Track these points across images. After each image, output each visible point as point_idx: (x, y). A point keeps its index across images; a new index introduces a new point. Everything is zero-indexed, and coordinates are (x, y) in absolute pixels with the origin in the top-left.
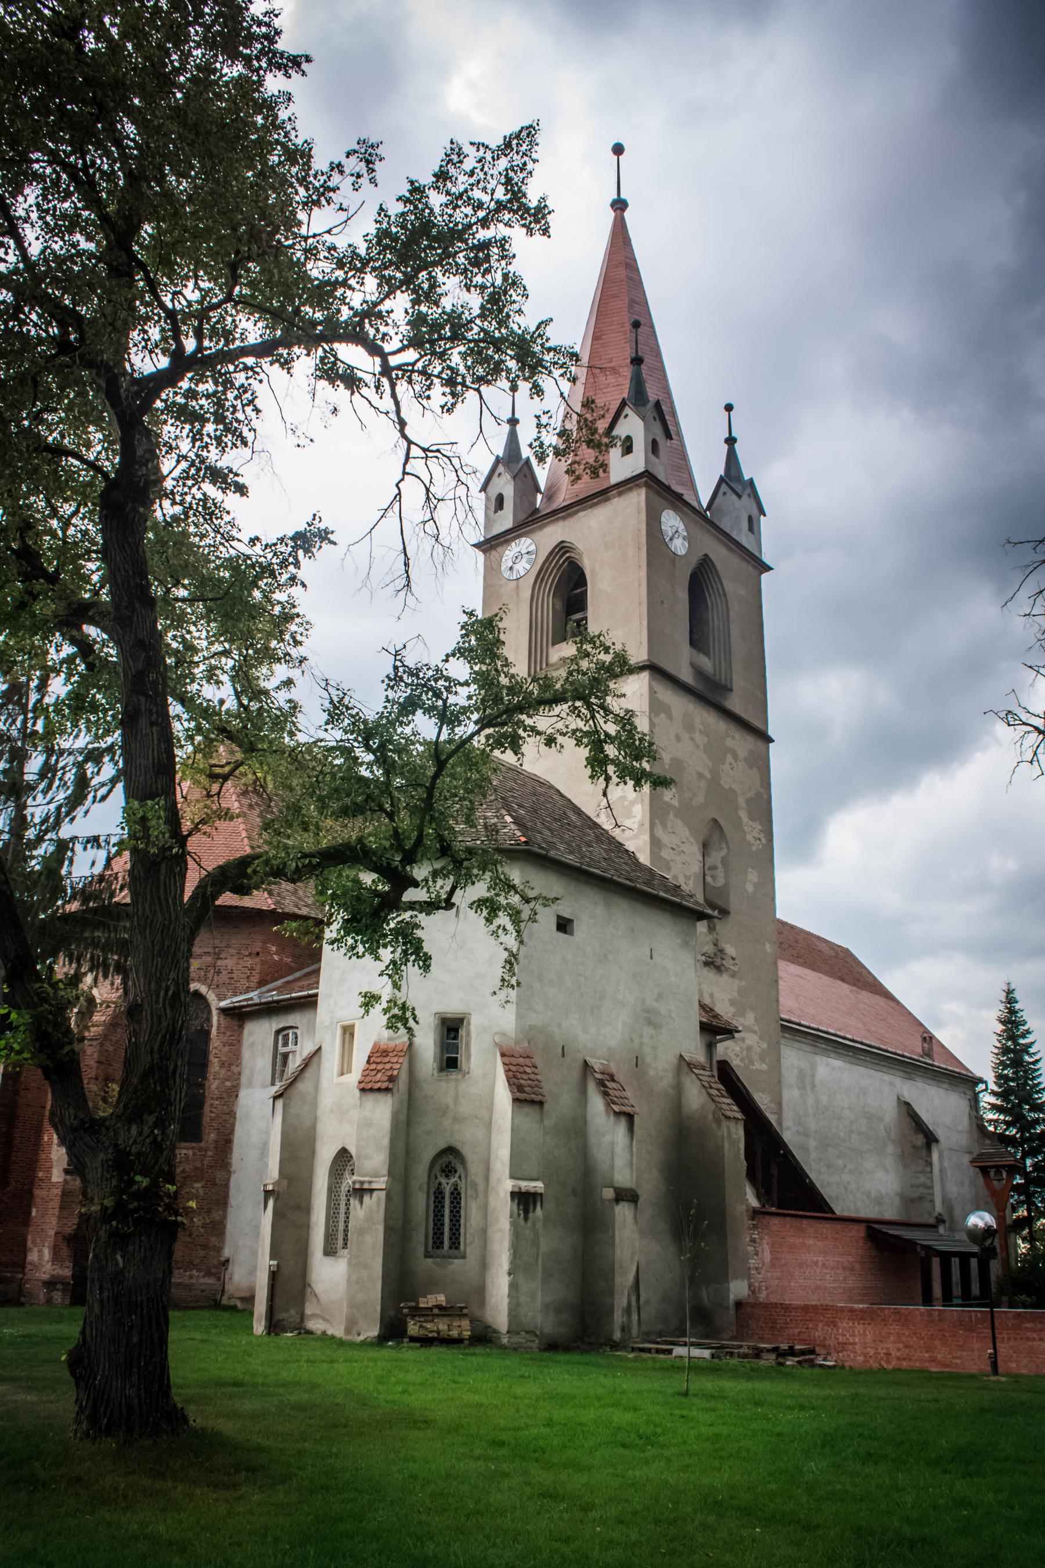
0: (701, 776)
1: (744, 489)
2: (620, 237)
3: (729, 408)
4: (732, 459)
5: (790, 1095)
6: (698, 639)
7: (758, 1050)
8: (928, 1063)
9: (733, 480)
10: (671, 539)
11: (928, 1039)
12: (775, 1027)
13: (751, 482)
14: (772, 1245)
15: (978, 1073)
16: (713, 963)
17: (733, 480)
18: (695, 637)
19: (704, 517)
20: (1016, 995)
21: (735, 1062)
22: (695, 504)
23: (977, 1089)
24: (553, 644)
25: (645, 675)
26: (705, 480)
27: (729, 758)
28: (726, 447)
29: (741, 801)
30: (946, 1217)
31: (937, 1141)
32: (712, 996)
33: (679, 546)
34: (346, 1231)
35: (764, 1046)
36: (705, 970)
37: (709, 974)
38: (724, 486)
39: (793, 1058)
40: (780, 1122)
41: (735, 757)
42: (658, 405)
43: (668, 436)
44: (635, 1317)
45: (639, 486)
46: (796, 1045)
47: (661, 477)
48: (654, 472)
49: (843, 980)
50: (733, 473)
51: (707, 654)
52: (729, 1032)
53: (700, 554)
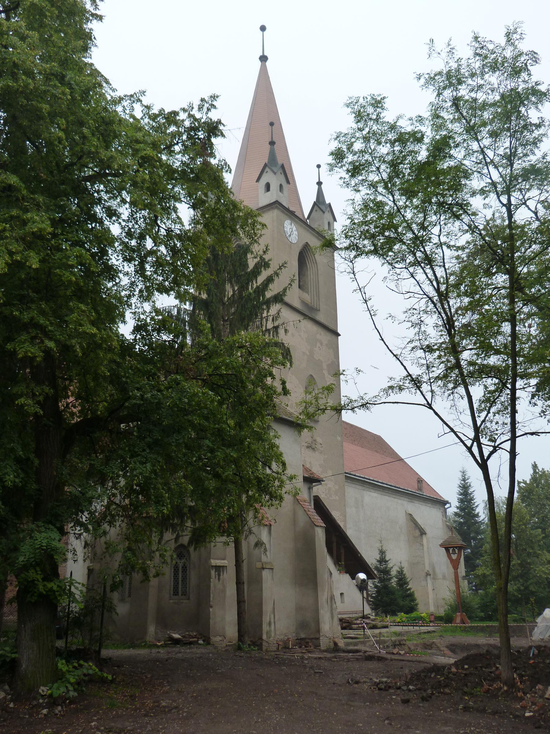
0: (304, 353)
1: (326, 208)
2: (264, 76)
4: (320, 194)
5: (351, 511)
8: (420, 493)
10: (290, 236)
11: (420, 481)
12: (342, 477)
13: (330, 205)
15: (446, 498)
16: (311, 447)
18: (301, 283)
19: (306, 223)
21: (322, 497)
22: (301, 217)
23: (446, 507)
27: (318, 344)
28: (317, 186)
29: (325, 366)
30: (431, 572)
31: (425, 534)
32: (310, 463)
33: (294, 238)
34: (130, 589)
35: (337, 487)
36: (307, 450)
37: (309, 452)
38: (316, 207)
39: (352, 492)
40: (345, 526)
41: (321, 344)
42: (283, 167)
43: (288, 182)
44: (273, 627)
46: (353, 485)
47: (284, 204)
48: (281, 201)
49: (377, 452)
50: (321, 200)
51: (307, 292)
52: (319, 481)
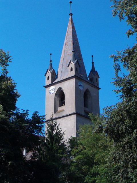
3: (92, 56)
4: (93, 67)
6: (85, 105)
7: (90, 125)
9: (93, 71)
14: (89, 117)
17: (93, 71)
20: (127, 37)
24: (59, 107)
25: (75, 115)
26: (88, 72)
45: (73, 78)
51: (88, 108)
53: (86, 89)
